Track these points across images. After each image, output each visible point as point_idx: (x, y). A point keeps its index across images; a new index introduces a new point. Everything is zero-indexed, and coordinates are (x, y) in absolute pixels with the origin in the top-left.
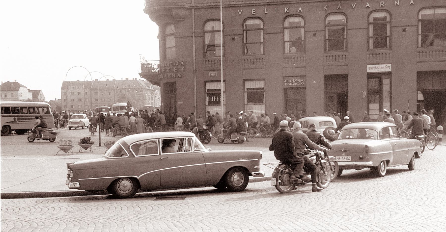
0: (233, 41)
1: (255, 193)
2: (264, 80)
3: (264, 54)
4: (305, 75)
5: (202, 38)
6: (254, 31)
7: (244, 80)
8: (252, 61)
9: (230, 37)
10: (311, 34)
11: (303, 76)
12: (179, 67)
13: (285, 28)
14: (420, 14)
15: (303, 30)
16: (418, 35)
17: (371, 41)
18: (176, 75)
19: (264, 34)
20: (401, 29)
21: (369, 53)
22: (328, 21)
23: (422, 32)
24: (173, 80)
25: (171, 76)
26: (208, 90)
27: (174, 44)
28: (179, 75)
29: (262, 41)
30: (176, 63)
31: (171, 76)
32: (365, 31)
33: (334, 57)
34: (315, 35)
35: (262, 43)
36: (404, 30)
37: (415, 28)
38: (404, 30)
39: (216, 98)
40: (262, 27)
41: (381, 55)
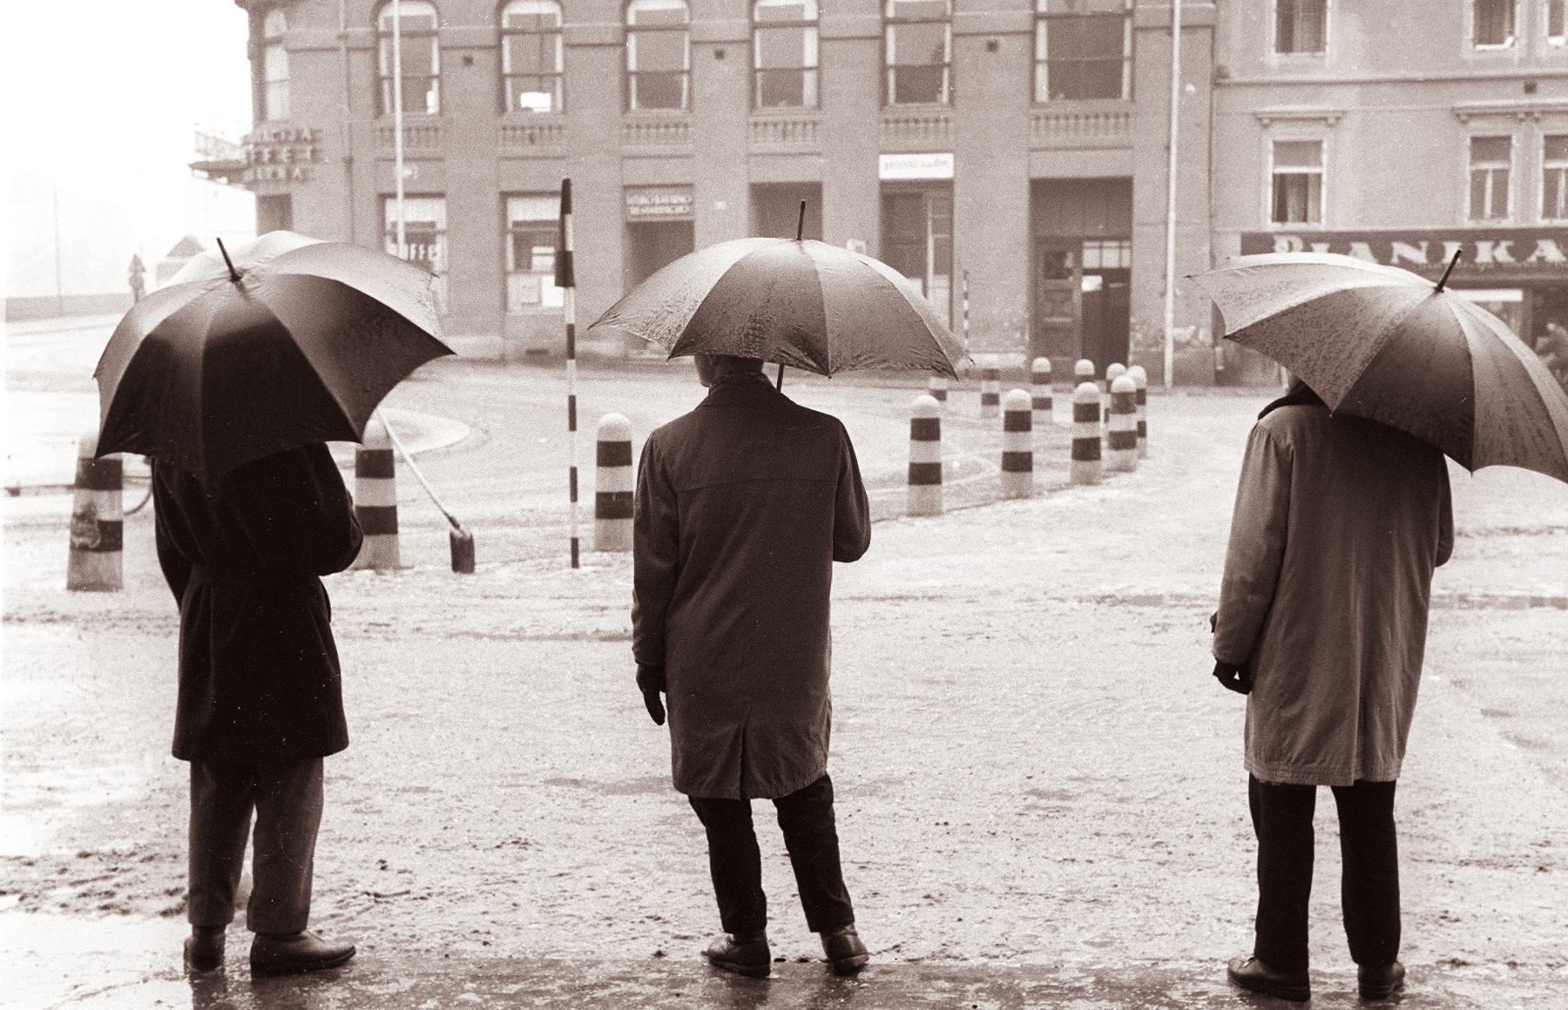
0: (466, 69)
1: (1276, 632)
2: (441, 195)
3: (819, 106)
4: (687, 179)
5: (619, 50)
6: (848, 35)
7: (505, 196)
8: (528, 132)
9: (458, 56)
10: (709, 52)
11: (687, 187)
12: (299, 147)
13: (628, 30)
14: (507, 13)
15: (810, 39)
16: (1034, 62)
17: (1042, 74)
18: (289, 173)
19: (569, 46)
20: (984, 40)
21: (629, 122)
22: (638, 13)
23: (1050, 50)
24: (283, 190)
25: (274, 174)
26: (516, 224)
27: (285, 75)
28: (297, 172)
29: (686, 66)
30: (288, 133)
31: (274, 174)
32: (871, 50)
33: (780, 127)
34: (720, 55)
35: (437, 76)
36: (992, 47)
37: (1026, 40)
38: (992, 47)
39: (417, 249)
40: (559, 24)
41: (932, 125)
